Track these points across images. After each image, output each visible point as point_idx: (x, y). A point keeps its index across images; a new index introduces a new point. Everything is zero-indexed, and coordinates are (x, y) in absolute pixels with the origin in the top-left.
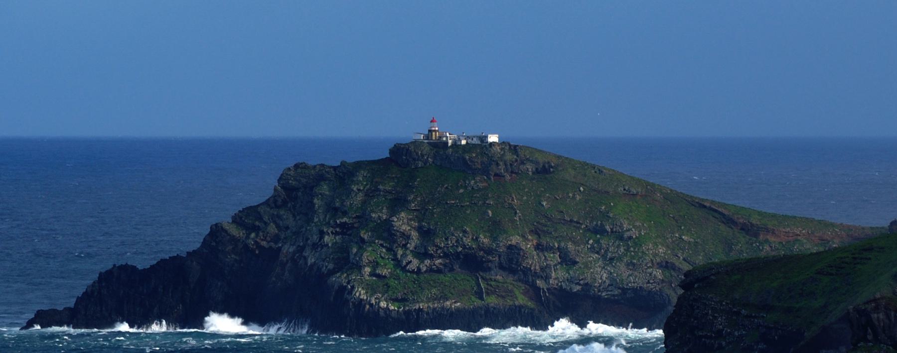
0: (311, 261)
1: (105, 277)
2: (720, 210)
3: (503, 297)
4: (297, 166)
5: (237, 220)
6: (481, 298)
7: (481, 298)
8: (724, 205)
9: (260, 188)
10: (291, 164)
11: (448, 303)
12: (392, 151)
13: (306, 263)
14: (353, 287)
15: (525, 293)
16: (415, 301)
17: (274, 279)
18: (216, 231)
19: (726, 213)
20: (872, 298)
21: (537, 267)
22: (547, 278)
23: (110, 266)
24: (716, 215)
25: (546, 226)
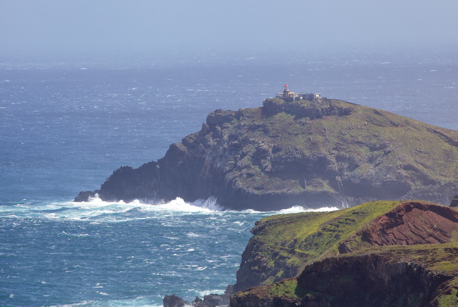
0: (219, 165)
1: (116, 173)
2: (445, 134)
3: (315, 186)
4: (216, 111)
5: (184, 141)
6: (304, 188)
7: (304, 188)
8: (449, 131)
9: (195, 126)
10: (213, 111)
11: (285, 190)
12: (264, 103)
13: (217, 167)
14: (236, 181)
15: (329, 184)
16: (268, 189)
17: (201, 175)
18: (173, 148)
19: (448, 135)
20: (446, 230)
21: (337, 168)
22: (341, 175)
23: (126, 166)
24: (442, 137)
25: (343, 145)
